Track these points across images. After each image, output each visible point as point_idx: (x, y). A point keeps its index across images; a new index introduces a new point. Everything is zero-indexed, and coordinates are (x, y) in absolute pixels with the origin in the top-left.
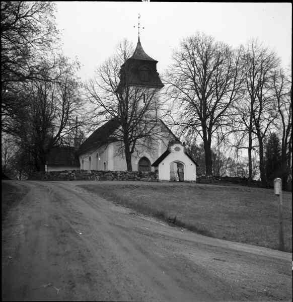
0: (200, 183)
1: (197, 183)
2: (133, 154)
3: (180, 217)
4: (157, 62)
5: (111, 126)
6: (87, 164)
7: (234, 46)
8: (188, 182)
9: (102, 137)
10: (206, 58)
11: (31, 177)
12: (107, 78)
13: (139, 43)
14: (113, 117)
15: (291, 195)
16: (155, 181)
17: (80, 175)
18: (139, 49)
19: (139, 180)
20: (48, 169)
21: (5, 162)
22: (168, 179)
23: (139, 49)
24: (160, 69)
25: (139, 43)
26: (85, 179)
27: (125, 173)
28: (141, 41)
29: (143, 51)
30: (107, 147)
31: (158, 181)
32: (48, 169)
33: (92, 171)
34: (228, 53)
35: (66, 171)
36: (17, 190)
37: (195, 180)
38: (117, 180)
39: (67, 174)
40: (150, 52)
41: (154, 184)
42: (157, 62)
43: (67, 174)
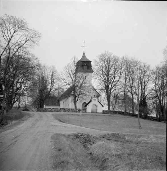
0: (104, 113)
1: (103, 113)
2: (78, 102)
3: (62, 120)
4: (91, 62)
5: (69, 91)
6: (63, 105)
7: (121, 57)
8: (99, 113)
9: (66, 95)
10: (108, 62)
11: (38, 110)
12: (68, 71)
13: (84, 53)
14: (70, 87)
15: (165, 125)
16: (85, 113)
17: (56, 110)
18: (84, 56)
19: (78, 112)
20: (45, 107)
21: (27, 102)
22: (91, 112)
23: (84, 56)
24: (92, 64)
25: (84, 53)
26: (57, 112)
27: (73, 109)
28: (85, 53)
29: (86, 57)
30: (67, 99)
31: (86, 113)
32: (45, 107)
33: (60, 108)
34: (116, 61)
35: (50, 108)
36: (31, 115)
37: (102, 112)
38: (70, 112)
39: (51, 109)
40: (89, 58)
41: (86, 114)
42: (91, 62)
43: (51, 109)
